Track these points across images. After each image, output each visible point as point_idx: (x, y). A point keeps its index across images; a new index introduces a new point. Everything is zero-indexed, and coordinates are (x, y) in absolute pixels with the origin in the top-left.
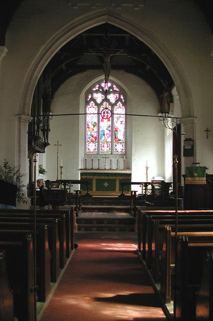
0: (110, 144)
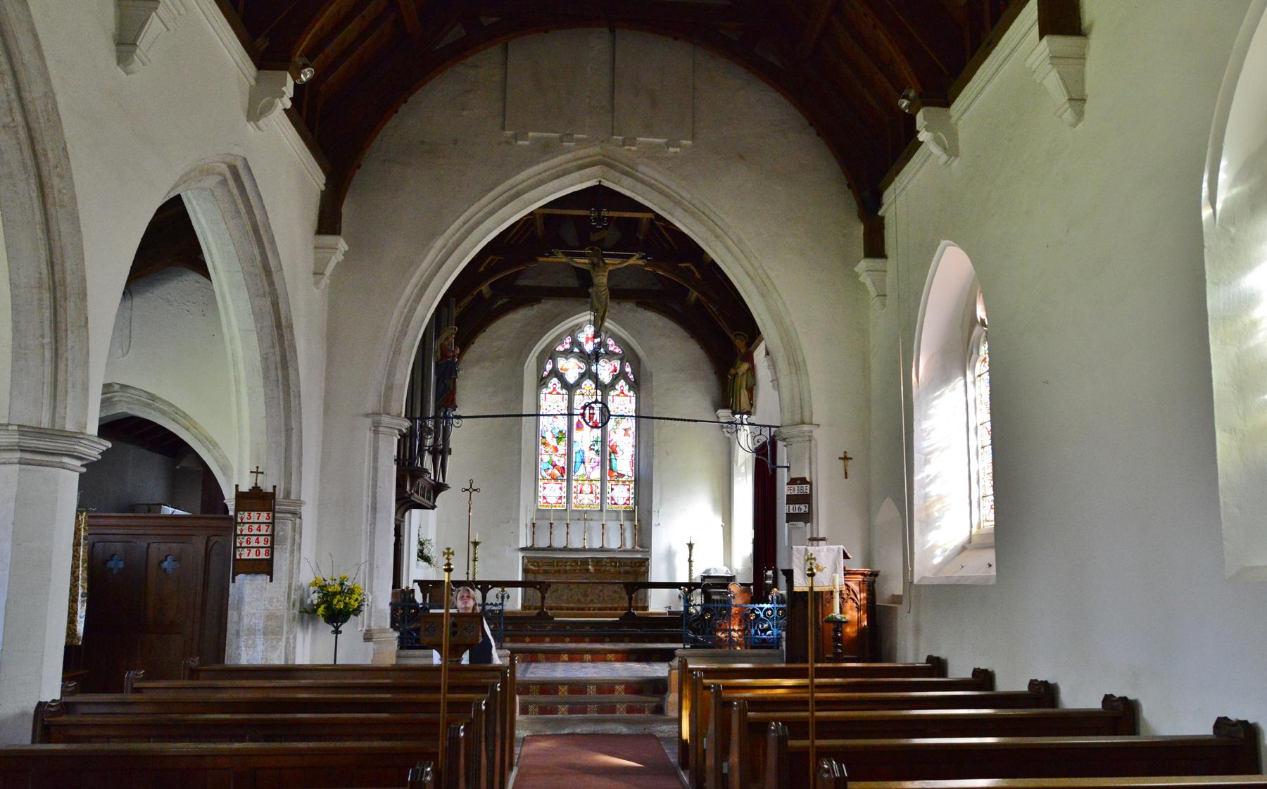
0: (599, 484)
